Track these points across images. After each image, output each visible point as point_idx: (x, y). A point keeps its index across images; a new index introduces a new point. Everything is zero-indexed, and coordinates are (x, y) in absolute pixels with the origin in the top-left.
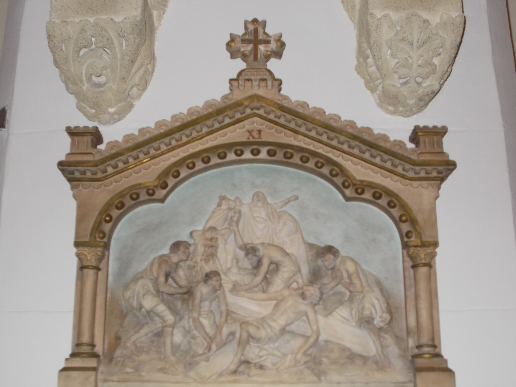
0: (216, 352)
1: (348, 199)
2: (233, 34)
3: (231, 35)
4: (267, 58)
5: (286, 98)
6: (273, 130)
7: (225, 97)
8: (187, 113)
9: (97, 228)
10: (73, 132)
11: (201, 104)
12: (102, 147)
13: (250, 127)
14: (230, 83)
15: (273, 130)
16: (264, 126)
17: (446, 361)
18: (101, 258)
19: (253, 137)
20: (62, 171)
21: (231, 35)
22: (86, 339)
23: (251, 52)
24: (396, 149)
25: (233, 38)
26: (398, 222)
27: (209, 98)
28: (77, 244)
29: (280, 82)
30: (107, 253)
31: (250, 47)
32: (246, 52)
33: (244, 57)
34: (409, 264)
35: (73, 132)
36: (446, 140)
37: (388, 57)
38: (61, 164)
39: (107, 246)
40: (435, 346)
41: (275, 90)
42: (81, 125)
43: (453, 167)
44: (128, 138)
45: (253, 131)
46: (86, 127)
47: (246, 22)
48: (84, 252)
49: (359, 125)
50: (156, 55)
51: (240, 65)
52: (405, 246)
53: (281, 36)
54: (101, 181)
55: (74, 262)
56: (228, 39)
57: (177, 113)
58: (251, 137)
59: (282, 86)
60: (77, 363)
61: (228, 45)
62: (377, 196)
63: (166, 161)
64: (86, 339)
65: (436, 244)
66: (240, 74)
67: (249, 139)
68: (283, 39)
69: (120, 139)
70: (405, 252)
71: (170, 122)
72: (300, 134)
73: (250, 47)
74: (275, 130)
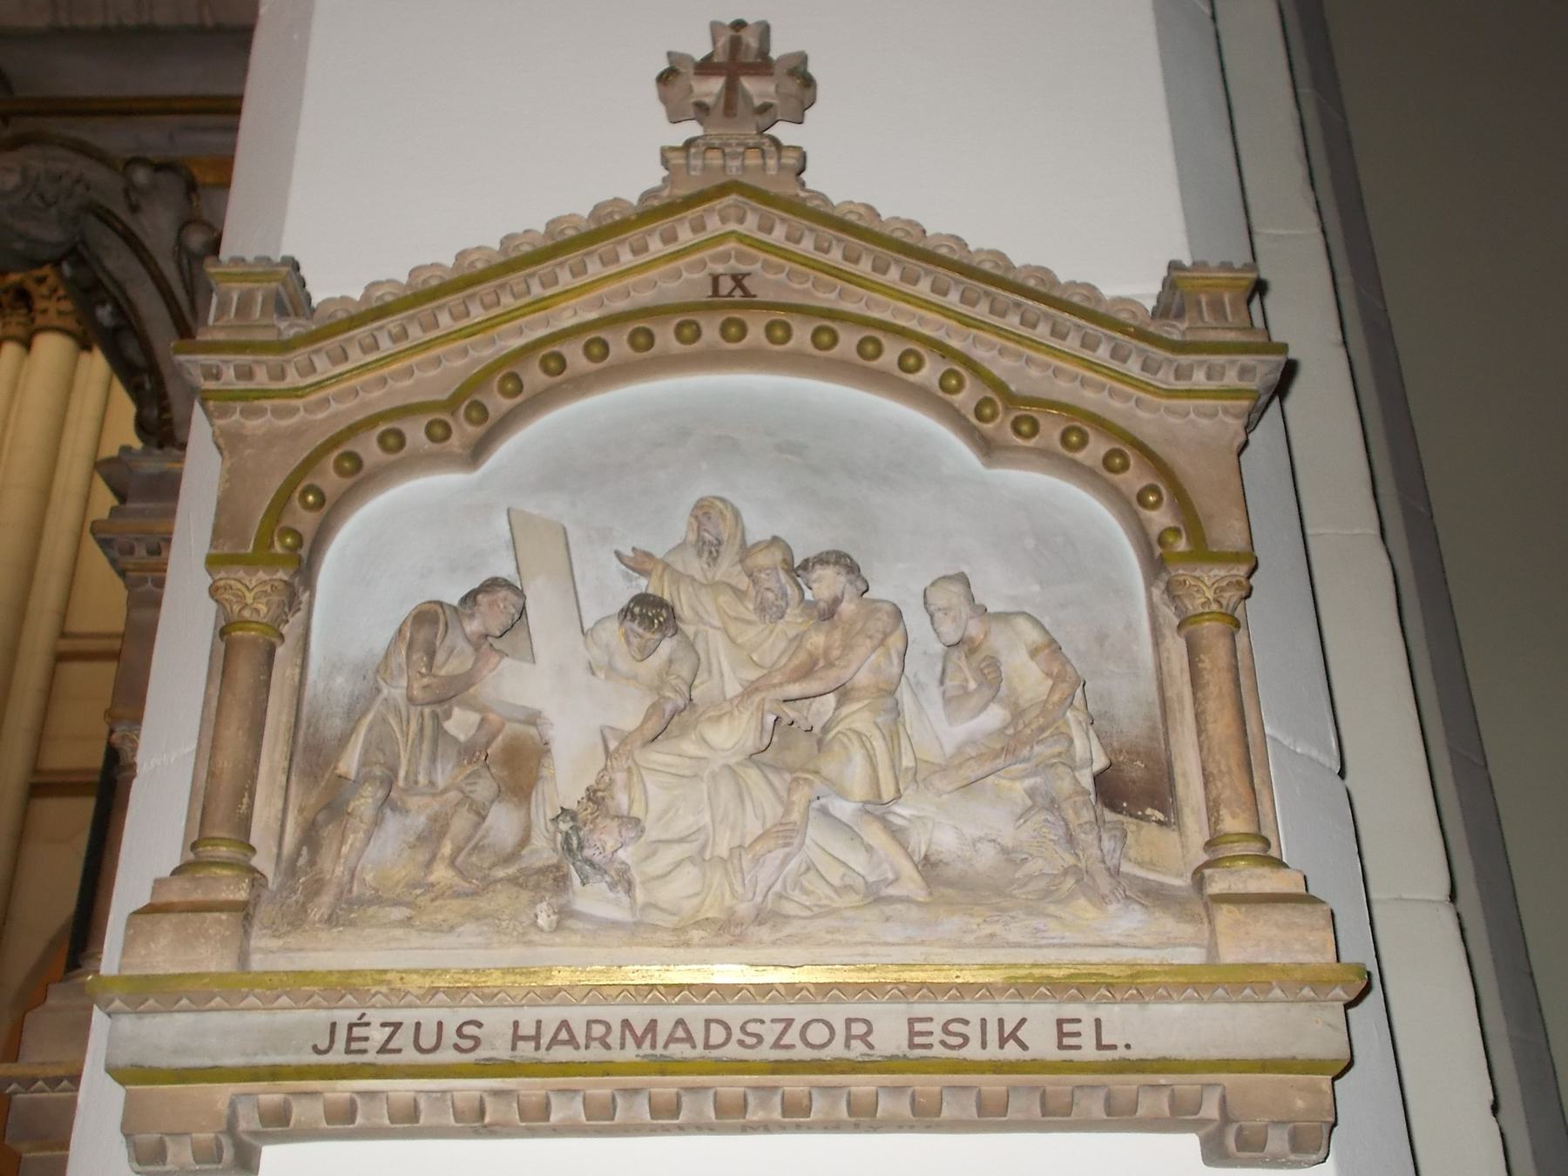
2: (676, 54)
3: (670, 54)
6: (809, 285)
8: (546, 232)
11: (585, 211)
15: (783, 276)
16: (758, 265)
21: (670, 54)
27: (606, 196)
30: (305, 597)
31: (716, 85)
32: (709, 101)
34: (1170, 616)
39: (304, 568)
47: (715, 27)
49: (1063, 277)
50: (611, 198)
56: (664, 65)
57: (519, 229)
59: (303, 272)
63: (262, 592)
68: (812, 69)
72: (1182, 391)
73: (716, 85)
74: (813, 285)
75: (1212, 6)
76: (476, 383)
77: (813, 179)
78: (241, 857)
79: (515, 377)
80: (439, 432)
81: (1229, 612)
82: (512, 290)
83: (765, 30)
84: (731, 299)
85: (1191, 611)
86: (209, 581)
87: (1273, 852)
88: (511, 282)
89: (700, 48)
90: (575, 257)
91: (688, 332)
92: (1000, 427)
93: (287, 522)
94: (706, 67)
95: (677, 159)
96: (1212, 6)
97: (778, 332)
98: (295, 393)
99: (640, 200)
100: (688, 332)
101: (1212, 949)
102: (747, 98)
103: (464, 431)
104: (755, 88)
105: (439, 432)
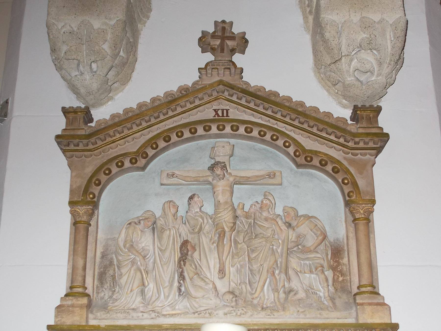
0: (117, 293)
1: (299, 166)
4: (233, 51)
5: (247, 83)
7: (195, 84)
9: (86, 191)
10: (65, 111)
11: (175, 89)
12: (93, 124)
13: (215, 107)
14: (200, 72)
17: (383, 298)
18: (91, 215)
19: (219, 116)
20: (59, 143)
21: (203, 32)
22: (78, 282)
23: (218, 46)
24: (341, 125)
25: (205, 34)
26: (341, 185)
28: (72, 203)
29: (242, 70)
31: (218, 42)
33: (213, 50)
34: (351, 218)
35: (65, 111)
36: (381, 118)
37: (108, 39)
38: (58, 137)
39: (95, 205)
40: (374, 287)
41: (237, 77)
42: (75, 106)
43: (386, 139)
44: (113, 116)
45: (218, 110)
46: (329, 114)
47: (216, 22)
48: (78, 210)
51: (209, 57)
52: (347, 204)
53: (244, 33)
54: (92, 151)
55: (67, 219)
56: (200, 35)
58: (216, 116)
60: (70, 301)
61: (200, 39)
62: (323, 163)
64: (78, 282)
65: (373, 202)
66: (207, 65)
67: (215, 116)
69: (108, 118)
70: (347, 210)
71: (150, 103)
73: (218, 42)
75: (403, 0)
76: (144, 145)
77: (246, 77)
78: (83, 291)
79: (156, 143)
80: (133, 161)
81: (367, 217)
82: (308, 124)
83: (231, 23)
84: (215, 118)
85: (357, 217)
86: (227, 21)
87: (376, 290)
88: (199, 96)
89: (211, 29)
90: (120, 128)
91: (207, 129)
92: (301, 160)
93: (91, 190)
94: (214, 36)
95: (203, 72)
96: (403, 0)
97: (235, 129)
98: (90, 150)
99: (192, 84)
100: (207, 129)
101: (357, 318)
102: (227, 45)
103: (141, 162)
104: (230, 43)
105: (133, 161)
